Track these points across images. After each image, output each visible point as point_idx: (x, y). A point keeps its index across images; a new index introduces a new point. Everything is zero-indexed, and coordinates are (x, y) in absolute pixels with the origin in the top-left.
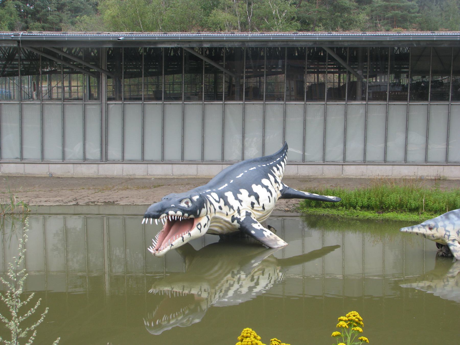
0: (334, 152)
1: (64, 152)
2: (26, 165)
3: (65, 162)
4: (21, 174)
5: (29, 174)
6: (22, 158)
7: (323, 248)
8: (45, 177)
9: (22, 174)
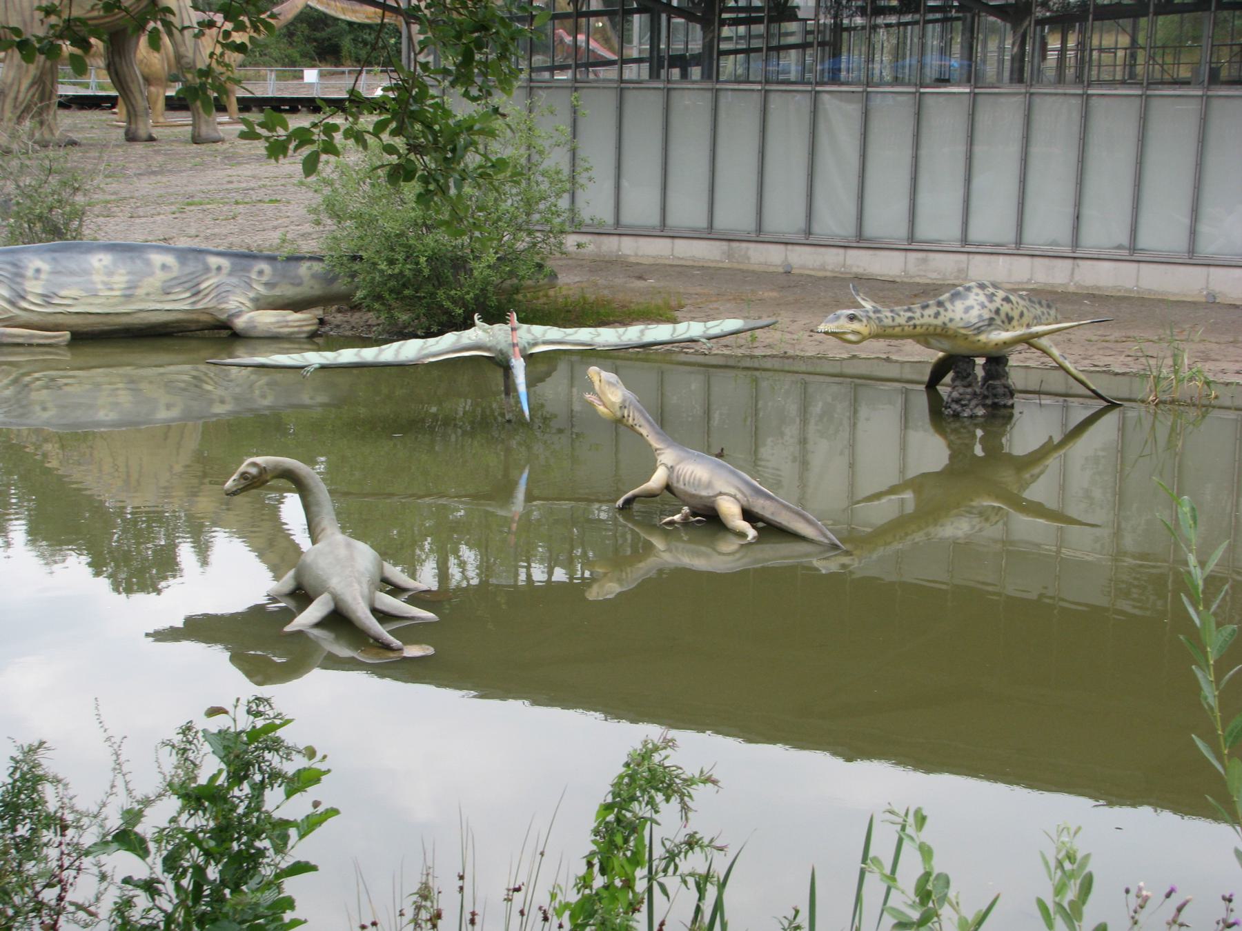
0: (1105, 227)
1: (1193, 233)
2: (1142, 265)
3: (812, 240)
4: (1126, 290)
5: (1150, 291)
6: (1133, 248)
7: (669, 446)
8: (1194, 303)
9: (1131, 291)
